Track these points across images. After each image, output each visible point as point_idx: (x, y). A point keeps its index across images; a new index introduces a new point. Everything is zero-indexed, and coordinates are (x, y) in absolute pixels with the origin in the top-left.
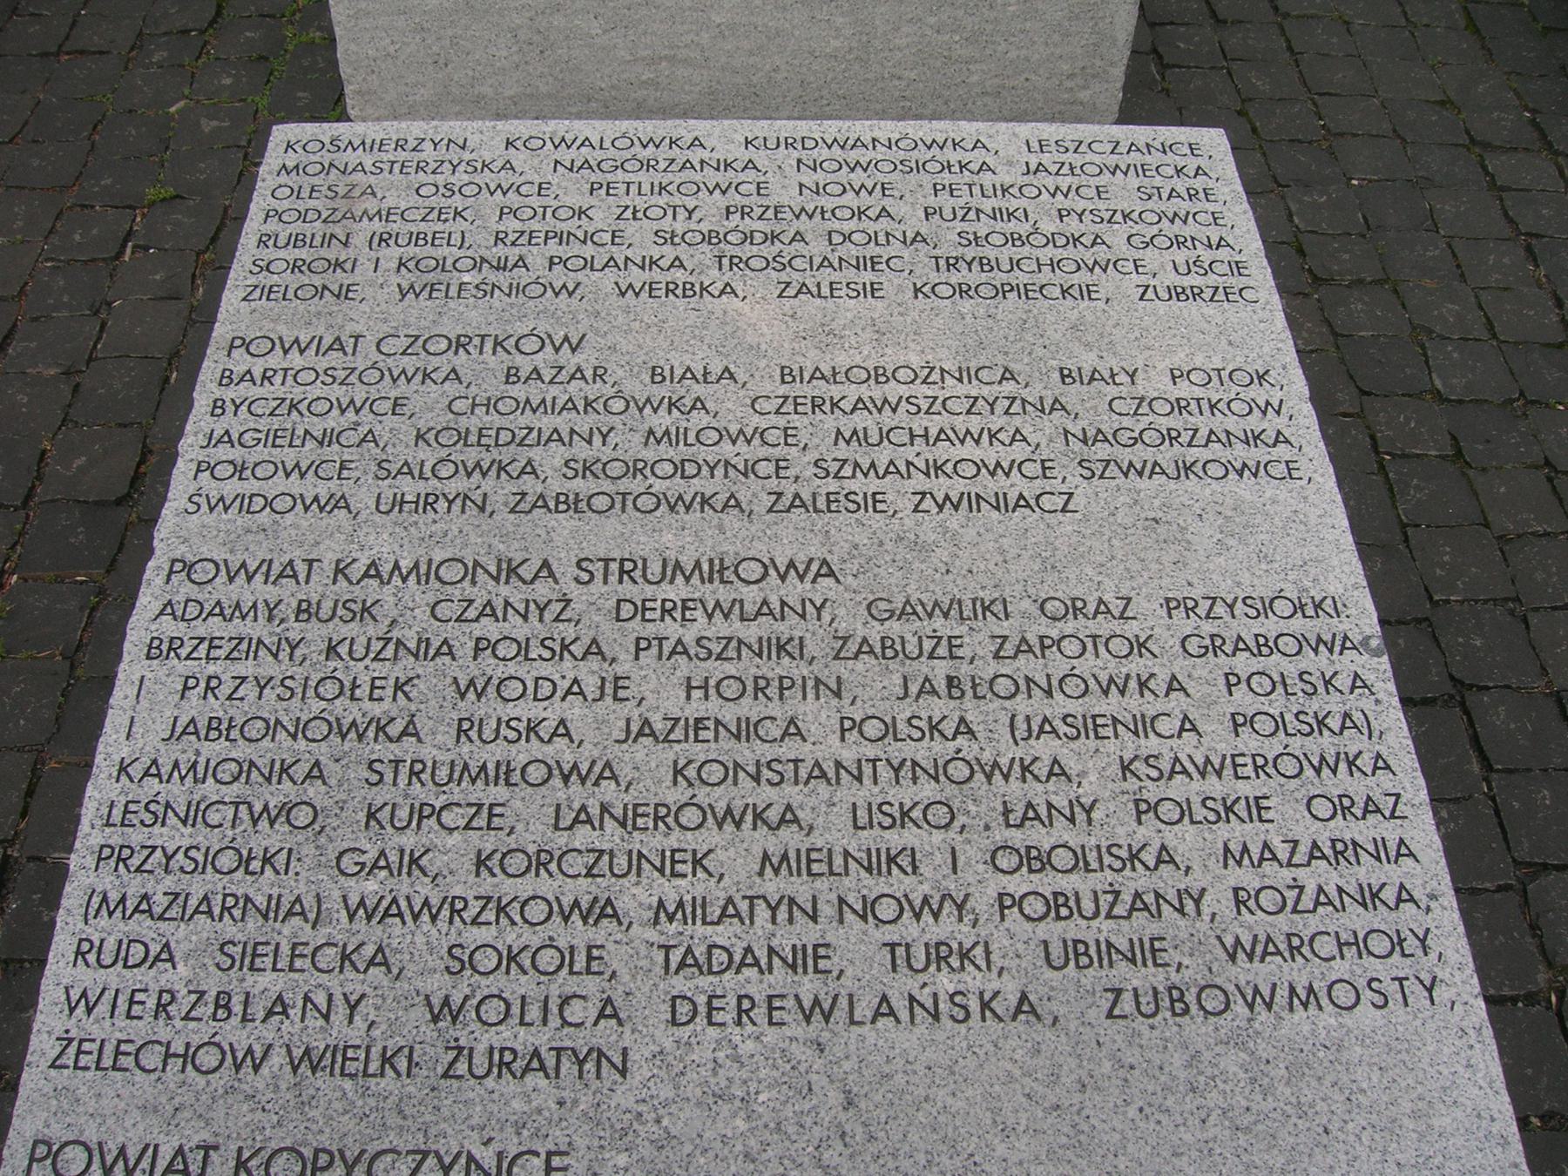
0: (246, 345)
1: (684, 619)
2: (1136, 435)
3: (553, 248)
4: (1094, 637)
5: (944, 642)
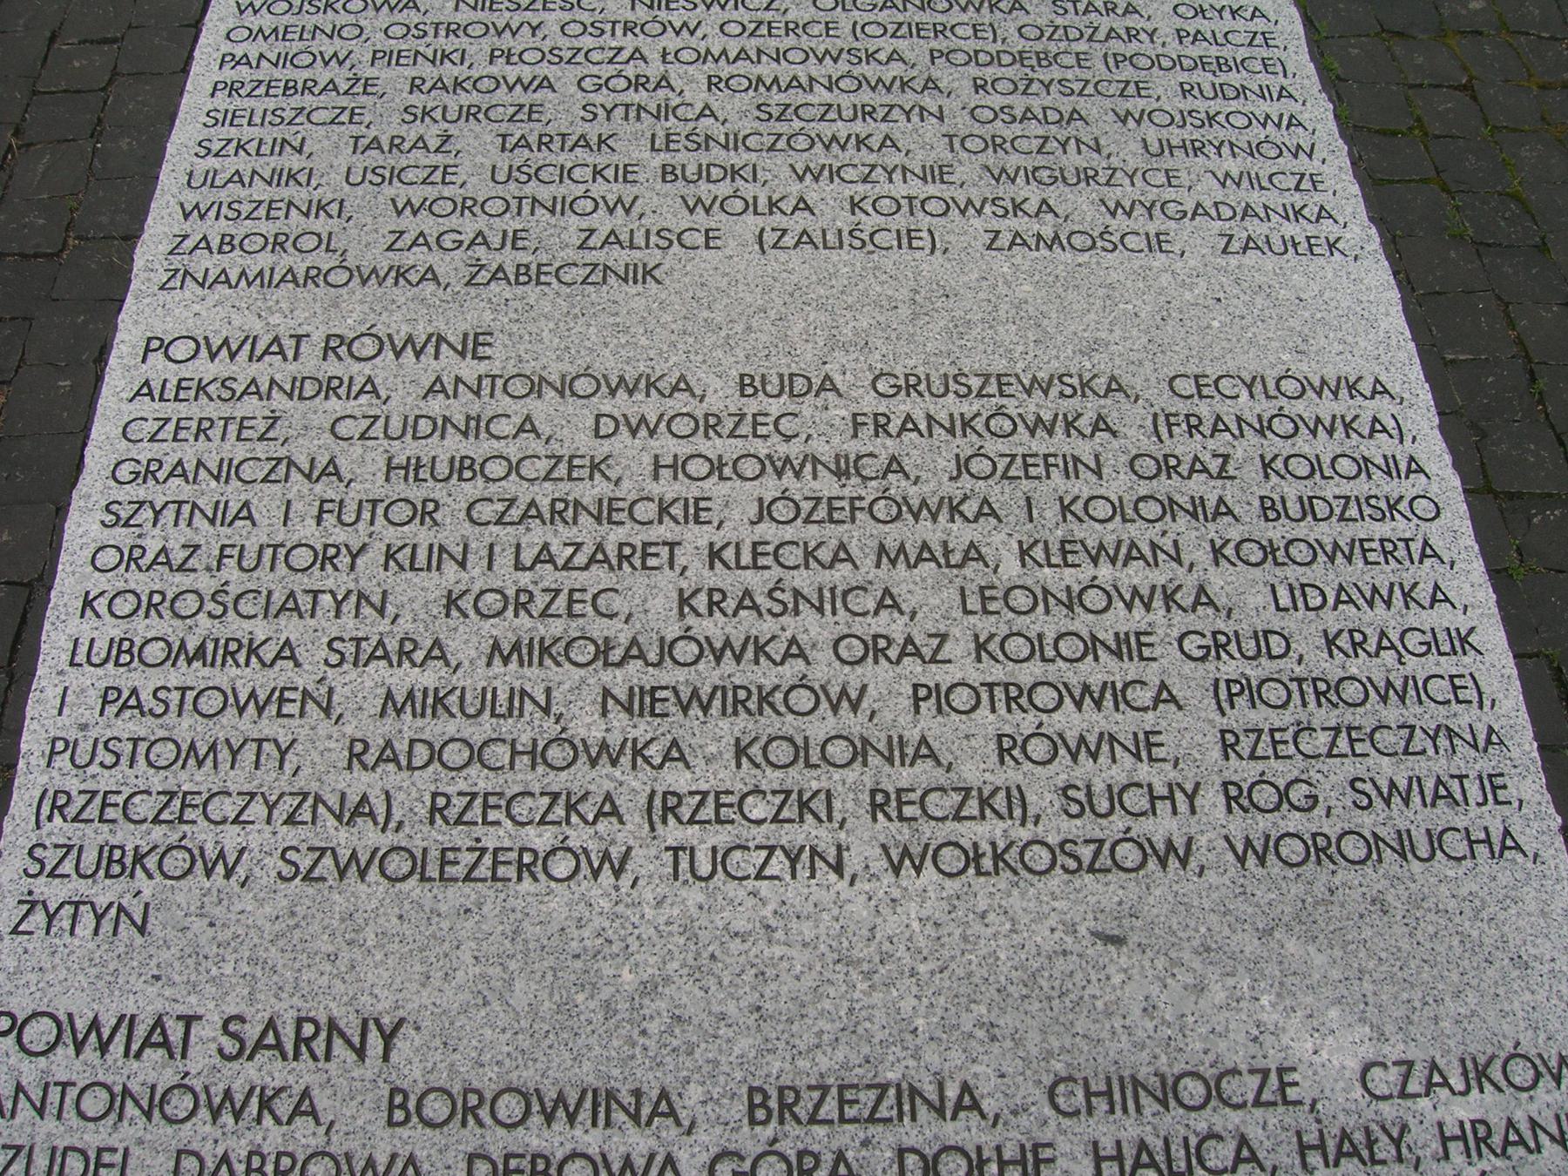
0: (165, 347)
1: (645, 567)
3: (491, 40)
4: (910, 198)
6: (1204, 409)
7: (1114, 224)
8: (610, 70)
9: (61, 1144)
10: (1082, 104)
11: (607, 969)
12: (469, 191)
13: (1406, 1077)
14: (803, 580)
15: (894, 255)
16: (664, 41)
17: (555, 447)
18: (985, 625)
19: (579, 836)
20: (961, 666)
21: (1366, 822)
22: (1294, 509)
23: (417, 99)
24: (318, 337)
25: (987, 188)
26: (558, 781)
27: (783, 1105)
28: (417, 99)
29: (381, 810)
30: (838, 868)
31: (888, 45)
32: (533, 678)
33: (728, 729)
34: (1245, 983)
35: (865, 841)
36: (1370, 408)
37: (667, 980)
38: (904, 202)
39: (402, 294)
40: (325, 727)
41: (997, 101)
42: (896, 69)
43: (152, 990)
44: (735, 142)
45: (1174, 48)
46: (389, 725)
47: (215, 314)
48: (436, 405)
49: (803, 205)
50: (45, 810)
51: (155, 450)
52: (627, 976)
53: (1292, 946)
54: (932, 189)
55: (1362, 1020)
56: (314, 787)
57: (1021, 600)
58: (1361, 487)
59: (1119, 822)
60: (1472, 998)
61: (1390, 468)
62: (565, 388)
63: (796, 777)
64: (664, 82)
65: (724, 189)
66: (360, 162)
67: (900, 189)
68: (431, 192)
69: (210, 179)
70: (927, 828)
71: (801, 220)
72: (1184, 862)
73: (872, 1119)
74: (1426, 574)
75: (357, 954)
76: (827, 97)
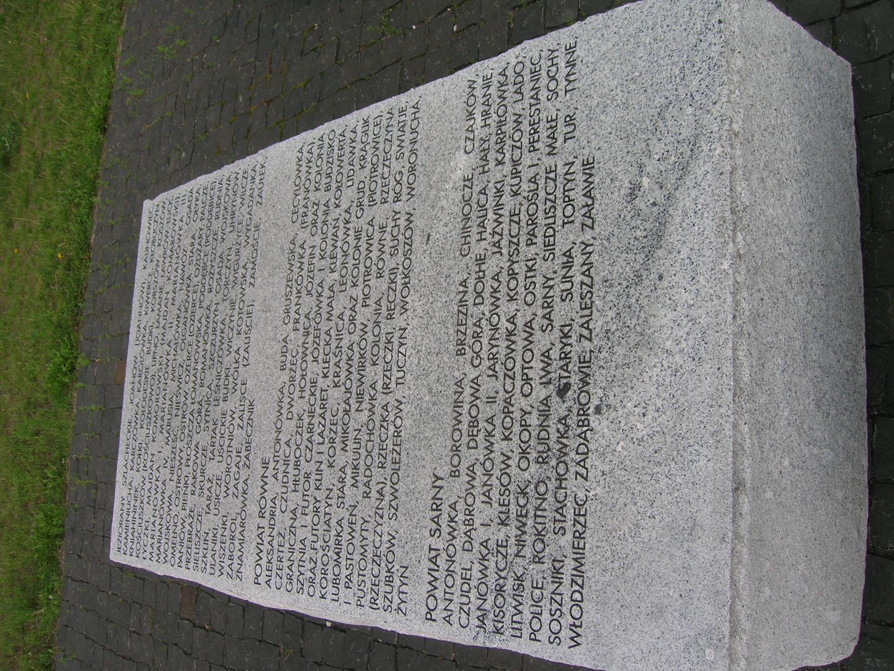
0: (430, 611)
2: (475, 355)
6: (301, 211)
7: (251, 243)
8: (195, 422)
9: (460, 593)
10: (218, 254)
11: (425, 405)
12: (223, 470)
13: (469, 139)
14: (333, 345)
15: (253, 318)
16: (189, 404)
17: (294, 434)
18: (349, 284)
19: (391, 418)
20: (357, 292)
21: (407, 154)
22: (328, 180)
23: (197, 492)
24: (259, 520)
25: (238, 287)
26: (378, 424)
27: (461, 344)
28: (197, 492)
29: (381, 485)
30: (405, 329)
31: (197, 323)
32: (352, 435)
33: (369, 368)
34: (442, 193)
35: (399, 321)
36: (306, 155)
37: (428, 385)
39: (250, 492)
40: (359, 507)
41: (215, 284)
42: (203, 320)
43: (422, 563)
44: (219, 375)
45: (205, 222)
46: (360, 485)
47: (248, 572)
48: (280, 476)
49: (237, 352)
50: (375, 606)
51: (284, 577)
52: (426, 399)
53: (435, 178)
54: (237, 307)
55: (454, 154)
56: (374, 509)
57: (344, 272)
58: (325, 157)
59: (401, 237)
60: (452, 118)
61: (321, 147)
62: (279, 431)
63: (382, 345)
64: (200, 403)
65: (231, 379)
66: (213, 511)
67: (236, 318)
68: (223, 484)
69: (213, 566)
70: (398, 301)
71: (242, 352)
72: (412, 215)
73: (466, 315)
74: (349, 135)
75: (416, 491)
76: (209, 344)
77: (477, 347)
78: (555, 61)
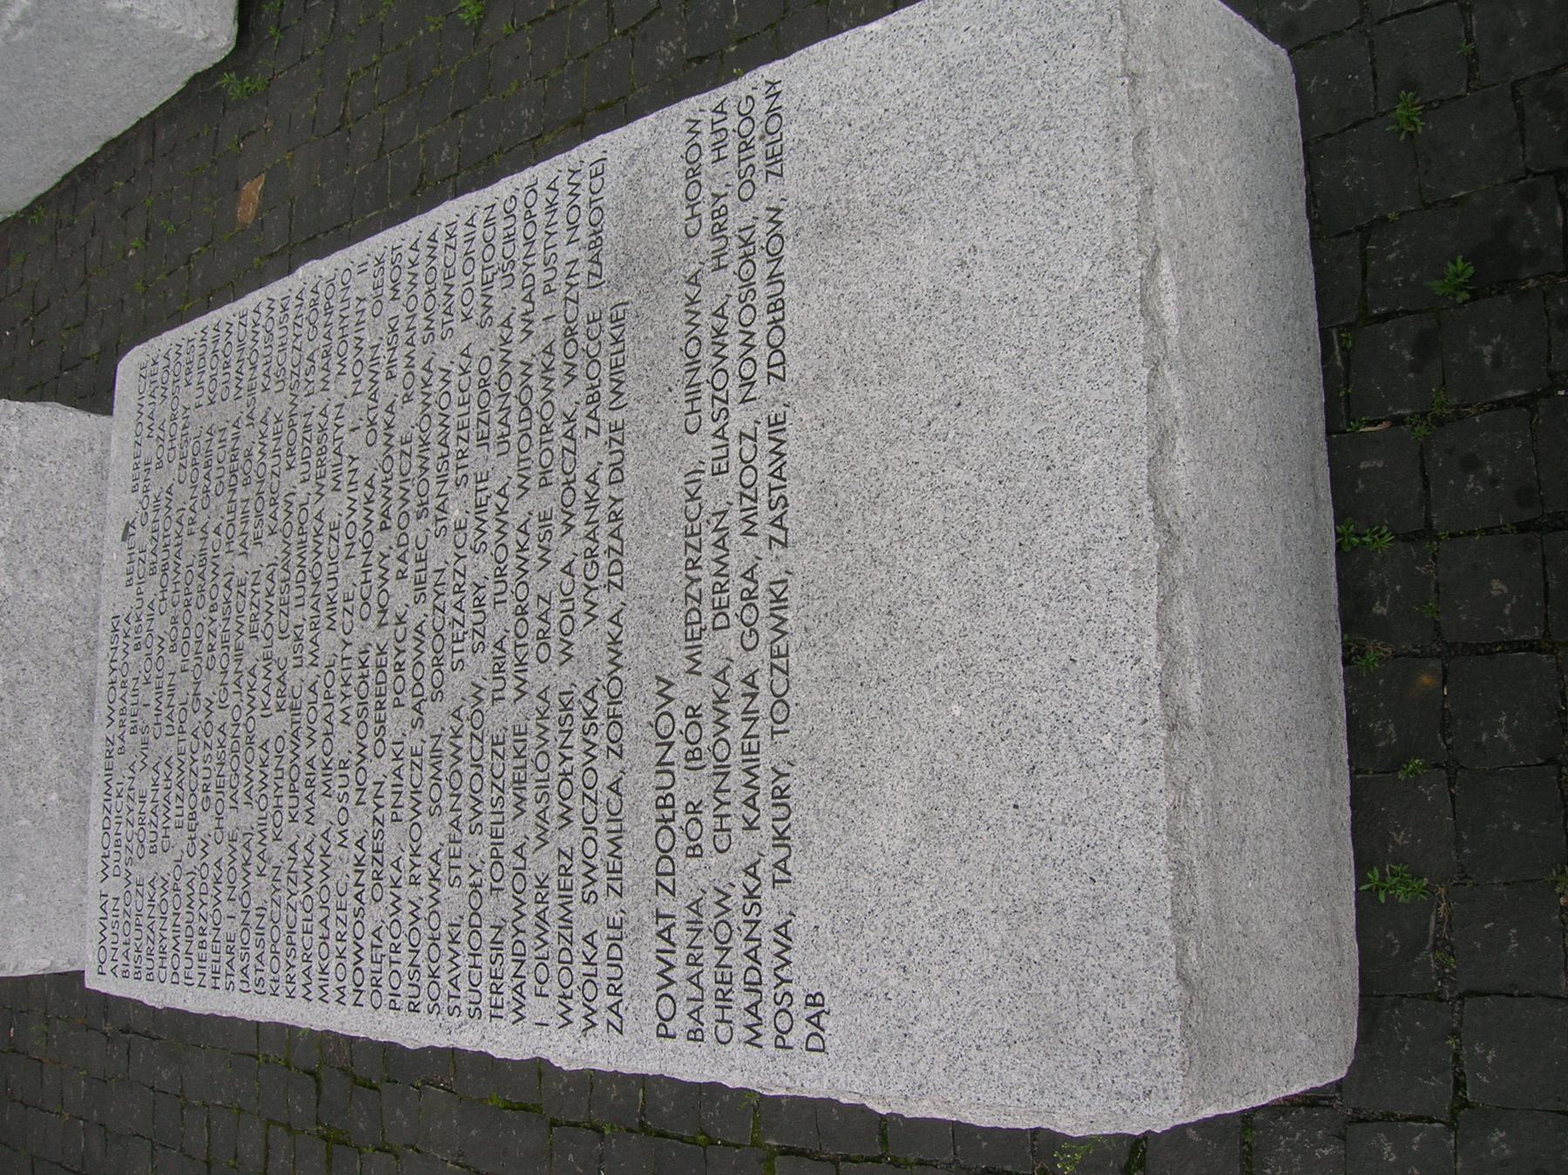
0: (664, 1021)
2: (747, 630)
5: (775, 661)
38: (544, 446)
77: (694, 734)
78: (696, 210)
